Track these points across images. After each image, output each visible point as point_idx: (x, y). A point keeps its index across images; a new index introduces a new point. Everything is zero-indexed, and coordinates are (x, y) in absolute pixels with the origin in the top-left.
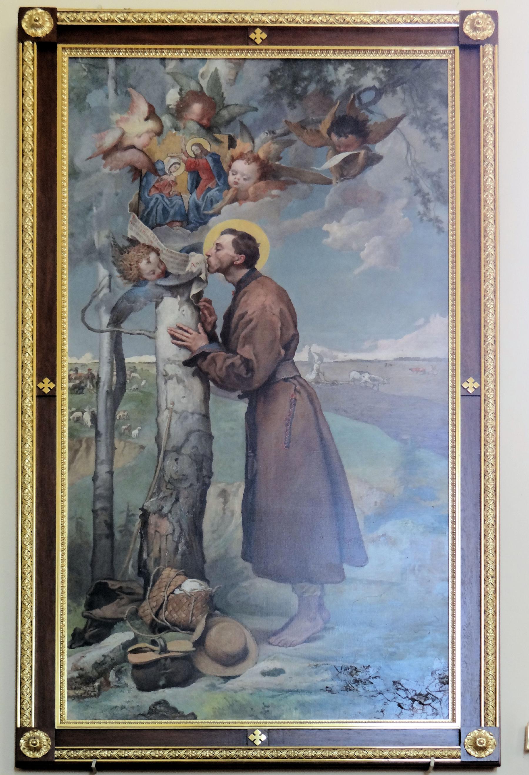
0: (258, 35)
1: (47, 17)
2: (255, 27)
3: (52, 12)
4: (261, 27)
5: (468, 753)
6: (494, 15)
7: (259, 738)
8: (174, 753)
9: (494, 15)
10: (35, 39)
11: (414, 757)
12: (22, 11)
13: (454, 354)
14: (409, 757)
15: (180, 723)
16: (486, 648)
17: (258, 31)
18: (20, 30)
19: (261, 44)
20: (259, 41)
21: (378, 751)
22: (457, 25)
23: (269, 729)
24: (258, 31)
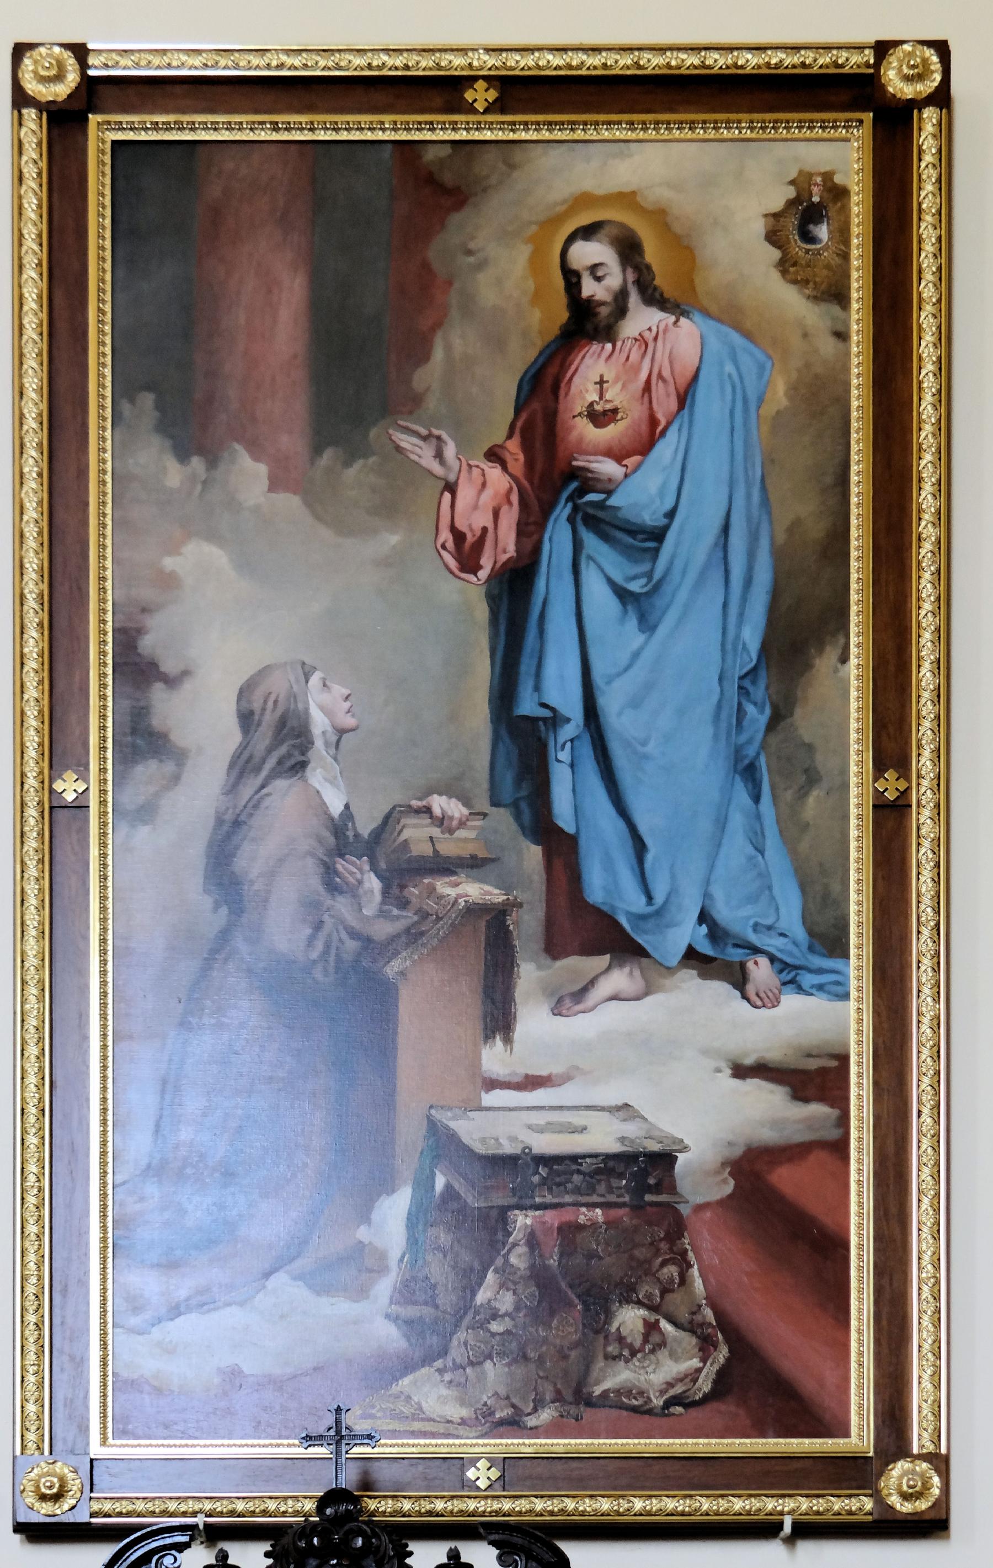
0: (480, 95)
1: (71, 62)
2: (475, 79)
3: (80, 52)
4: (485, 78)
5: (70, 1510)
6: (942, 48)
7: (481, 1475)
8: (723, 1504)
9: (942, 48)
10: (40, 107)
11: (129, 1514)
12: (20, 51)
13: (103, 835)
14: (120, 1514)
15: (278, 1446)
16: (40, 1337)
17: (480, 85)
18: (18, 89)
19: (486, 111)
20: (480, 107)
21: (290, 1502)
22: (871, 71)
23: (505, 1458)
24: (480, 85)
